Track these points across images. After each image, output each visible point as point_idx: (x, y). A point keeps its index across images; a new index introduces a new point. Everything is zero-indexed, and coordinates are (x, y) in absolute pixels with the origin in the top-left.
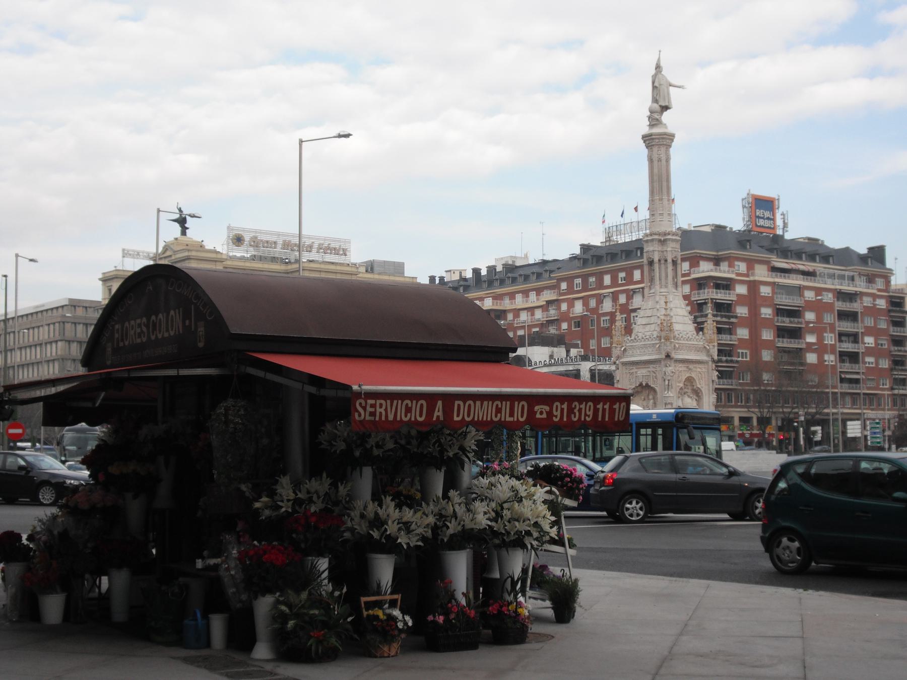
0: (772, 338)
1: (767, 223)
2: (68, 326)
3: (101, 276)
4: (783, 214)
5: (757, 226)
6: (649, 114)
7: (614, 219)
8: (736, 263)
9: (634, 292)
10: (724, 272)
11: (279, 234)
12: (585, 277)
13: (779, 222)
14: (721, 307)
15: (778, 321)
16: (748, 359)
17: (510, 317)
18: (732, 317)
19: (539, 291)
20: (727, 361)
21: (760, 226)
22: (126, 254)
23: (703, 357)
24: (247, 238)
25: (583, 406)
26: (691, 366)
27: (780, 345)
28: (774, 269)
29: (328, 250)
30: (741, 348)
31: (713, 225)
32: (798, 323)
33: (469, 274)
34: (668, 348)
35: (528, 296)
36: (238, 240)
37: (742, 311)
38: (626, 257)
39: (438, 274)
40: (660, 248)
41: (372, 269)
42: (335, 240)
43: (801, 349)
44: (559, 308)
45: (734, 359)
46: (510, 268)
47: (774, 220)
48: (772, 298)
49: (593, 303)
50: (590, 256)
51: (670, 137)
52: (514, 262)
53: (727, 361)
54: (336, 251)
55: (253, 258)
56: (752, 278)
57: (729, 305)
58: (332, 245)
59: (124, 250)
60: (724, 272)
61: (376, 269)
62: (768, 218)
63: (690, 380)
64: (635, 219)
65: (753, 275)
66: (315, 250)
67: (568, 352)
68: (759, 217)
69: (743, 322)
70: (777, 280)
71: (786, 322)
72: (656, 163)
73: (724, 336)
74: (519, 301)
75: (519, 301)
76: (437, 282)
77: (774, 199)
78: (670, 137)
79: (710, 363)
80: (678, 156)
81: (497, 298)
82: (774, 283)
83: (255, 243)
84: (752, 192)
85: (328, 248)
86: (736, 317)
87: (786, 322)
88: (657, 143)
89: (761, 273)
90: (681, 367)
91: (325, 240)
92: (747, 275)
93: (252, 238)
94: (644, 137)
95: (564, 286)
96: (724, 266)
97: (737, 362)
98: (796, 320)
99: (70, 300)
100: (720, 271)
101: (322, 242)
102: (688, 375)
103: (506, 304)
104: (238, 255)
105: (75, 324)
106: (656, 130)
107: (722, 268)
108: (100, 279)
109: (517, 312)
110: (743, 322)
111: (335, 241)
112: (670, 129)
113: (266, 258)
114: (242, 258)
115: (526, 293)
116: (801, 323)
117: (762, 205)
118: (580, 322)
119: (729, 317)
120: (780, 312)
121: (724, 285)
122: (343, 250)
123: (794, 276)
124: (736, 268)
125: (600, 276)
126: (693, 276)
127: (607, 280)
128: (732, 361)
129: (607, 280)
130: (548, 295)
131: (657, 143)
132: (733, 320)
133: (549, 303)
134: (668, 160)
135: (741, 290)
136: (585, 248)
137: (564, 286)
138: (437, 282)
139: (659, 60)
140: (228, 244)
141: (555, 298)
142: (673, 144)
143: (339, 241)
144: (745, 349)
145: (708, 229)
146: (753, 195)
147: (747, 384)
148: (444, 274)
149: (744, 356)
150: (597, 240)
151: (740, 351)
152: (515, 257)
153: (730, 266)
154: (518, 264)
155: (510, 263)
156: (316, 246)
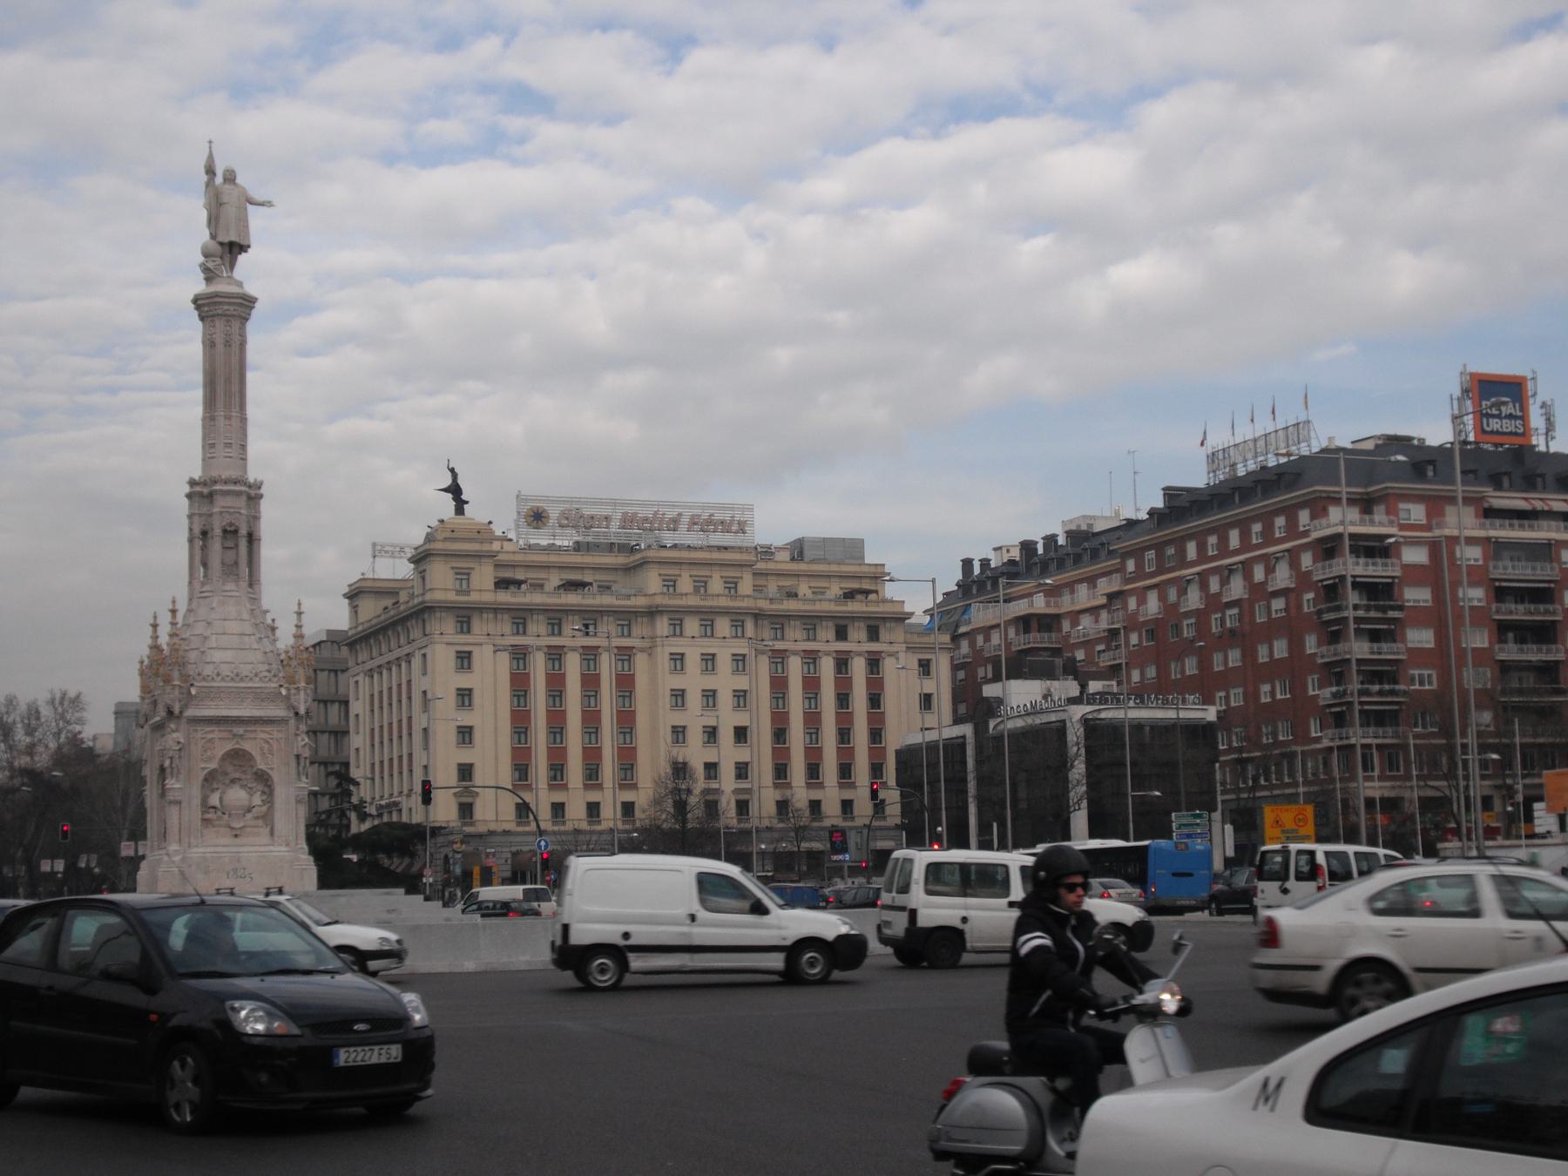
0: (1486, 645)
1: (1508, 426)
2: (322, 676)
3: (346, 590)
4: (1544, 405)
5: (1484, 432)
6: (201, 259)
7: (1219, 439)
8: (1402, 506)
9: (1231, 571)
10: (1381, 524)
11: (614, 503)
12: (1159, 547)
13: (1536, 420)
14: (1377, 592)
15: (1498, 612)
16: (1435, 686)
17: (1066, 625)
18: (1393, 608)
19: (1091, 581)
20: (1380, 693)
21: (1492, 432)
22: (377, 551)
23: (278, 711)
24: (553, 514)
25: (801, 795)
26: (240, 730)
27: (1502, 656)
28: (1490, 513)
29: (707, 524)
30: (1419, 667)
31: (1379, 438)
32: (1547, 612)
33: (1016, 554)
34: (172, 697)
35: (1095, 586)
36: (537, 518)
37: (1416, 596)
38: (1241, 500)
39: (977, 557)
40: (204, 510)
41: (801, 553)
42: (723, 507)
43: (1557, 663)
44: (1125, 607)
45: (1402, 687)
46: (1079, 537)
47: (1524, 418)
48: (1485, 568)
49: (1172, 595)
50: (1181, 506)
51: (248, 302)
52: (1090, 526)
53: (1380, 693)
54: (725, 526)
55: (578, 547)
56: (1437, 532)
57: (1389, 587)
58: (718, 516)
59: (374, 545)
60: (1379, 525)
61: (808, 554)
62: (1510, 416)
63: (238, 757)
64: (1270, 429)
65: (1440, 526)
66: (683, 527)
67: (1083, 687)
68: (1489, 416)
69: (1420, 617)
70: (1492, 533)
71: (1518, 612)
72: (220, 347)
73: (1385, 646)
74: (1083, 597)
75: (1083, 597)
76: (977, 571)
77: (1524, 379)
78: (248, 302)
79: (292, 722)
80: (259, 340)
81: (1052, 592)
82: (1488, 539)
83: (572, 519)
84: (1472, 369)
85: (709, 522)
86: (1401, 608)
87: (1518, 612)
88: (224, 314)
89: (1461, 522)
90: (216, 733)
91: (703, 508)
92: (1428, 528)
93: (563, 513)
94: (198, 302)
95: (1131, 565)
96: (1379, 513)
97: (1405, 693)
98: (1542, 607)
99: (329, 632)
100: (1372, 523)
101: (698, 512)
102: (229, 746)
103: (1066, 604)
104: (544, 542)
105: (336, 672)
106: (220, 287)
107: (1377, 518)
108: (345, 596)
109: (1075, 616)
110: (1420, 617)
111: (724, 508)
112: (250, 289)
113: (597, 546)
114: (551, 548)
115: (1091, 581)
116: (1554, 613)
117: (1496, 393)
118: (1154, 629)
119: (1384, 609)
120: (1500, 593)
121: (1373, 548)
122: (739, 523)
123: (1544, 523)
124: (1402, 515)
125: (1180, 542)
126: (1315, 535)
127: (1191, 550)
128: (1392, 693)
129: (1191, 550)
130: (1106, 586)
131: (224, 314)
132: (1391, 614)
133: (1112, 597)
134: (243, 344)
135: (1415, 556)
136: (1170, 493)
137: (1131, 565)
138: (977, 571)
139: (211, 157)
140: (518, 526)
141: (1116, 589)
142: (254, 312)
143: (732, 509)
144: (1426, 667)
145: (1369, 445)
146: (1472, 375)
147: (1432, 735)
148: (991, 555)
149: (1423, 680)
150: (1197, 477)
151: (1416, 672)
152: (1094, 518)
153: (1388, 513)
154: (1097, 529)
155: (1084, 527)
156: (685, 520)
